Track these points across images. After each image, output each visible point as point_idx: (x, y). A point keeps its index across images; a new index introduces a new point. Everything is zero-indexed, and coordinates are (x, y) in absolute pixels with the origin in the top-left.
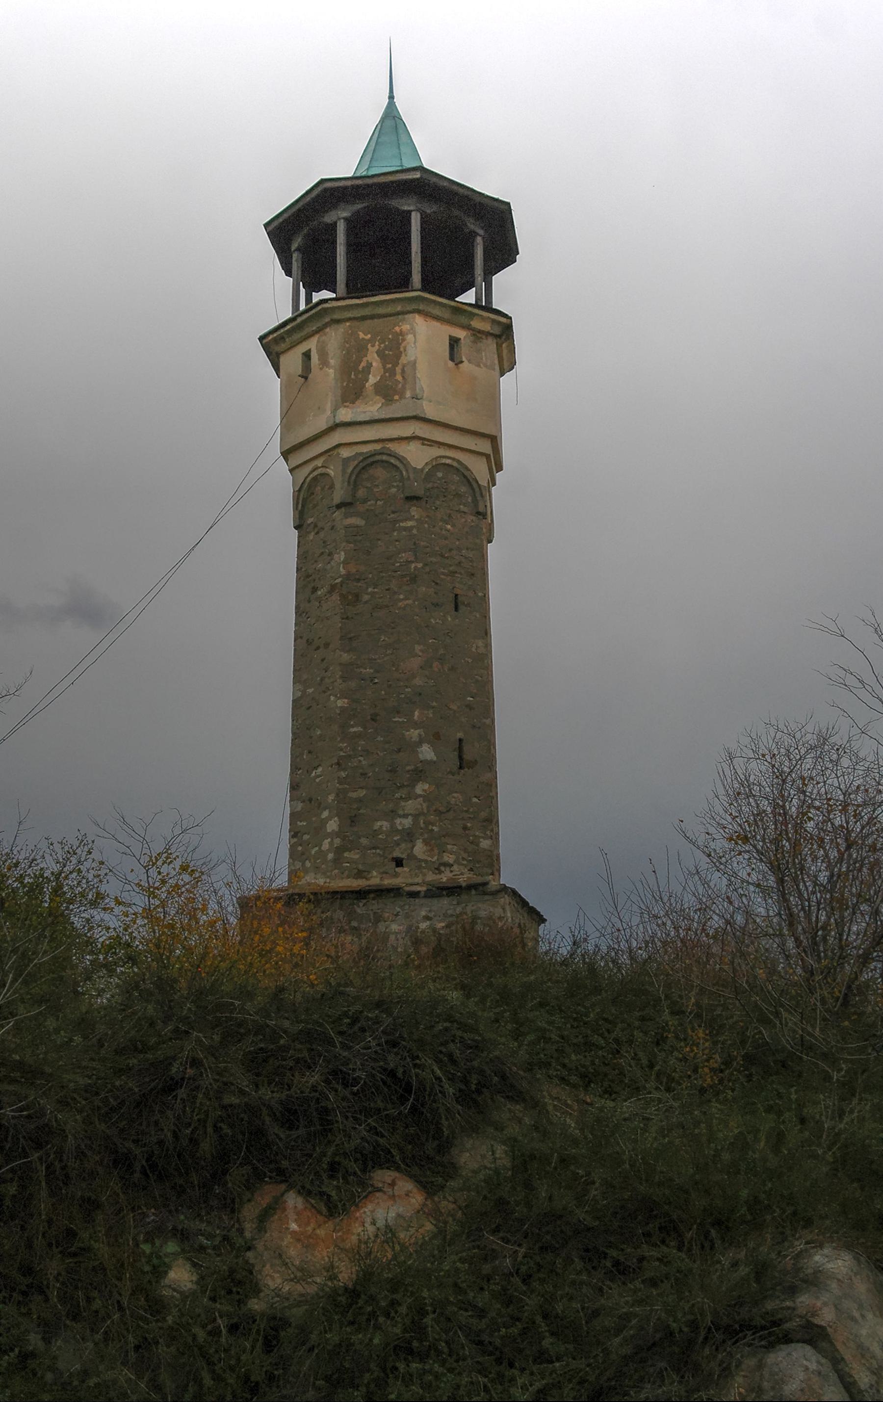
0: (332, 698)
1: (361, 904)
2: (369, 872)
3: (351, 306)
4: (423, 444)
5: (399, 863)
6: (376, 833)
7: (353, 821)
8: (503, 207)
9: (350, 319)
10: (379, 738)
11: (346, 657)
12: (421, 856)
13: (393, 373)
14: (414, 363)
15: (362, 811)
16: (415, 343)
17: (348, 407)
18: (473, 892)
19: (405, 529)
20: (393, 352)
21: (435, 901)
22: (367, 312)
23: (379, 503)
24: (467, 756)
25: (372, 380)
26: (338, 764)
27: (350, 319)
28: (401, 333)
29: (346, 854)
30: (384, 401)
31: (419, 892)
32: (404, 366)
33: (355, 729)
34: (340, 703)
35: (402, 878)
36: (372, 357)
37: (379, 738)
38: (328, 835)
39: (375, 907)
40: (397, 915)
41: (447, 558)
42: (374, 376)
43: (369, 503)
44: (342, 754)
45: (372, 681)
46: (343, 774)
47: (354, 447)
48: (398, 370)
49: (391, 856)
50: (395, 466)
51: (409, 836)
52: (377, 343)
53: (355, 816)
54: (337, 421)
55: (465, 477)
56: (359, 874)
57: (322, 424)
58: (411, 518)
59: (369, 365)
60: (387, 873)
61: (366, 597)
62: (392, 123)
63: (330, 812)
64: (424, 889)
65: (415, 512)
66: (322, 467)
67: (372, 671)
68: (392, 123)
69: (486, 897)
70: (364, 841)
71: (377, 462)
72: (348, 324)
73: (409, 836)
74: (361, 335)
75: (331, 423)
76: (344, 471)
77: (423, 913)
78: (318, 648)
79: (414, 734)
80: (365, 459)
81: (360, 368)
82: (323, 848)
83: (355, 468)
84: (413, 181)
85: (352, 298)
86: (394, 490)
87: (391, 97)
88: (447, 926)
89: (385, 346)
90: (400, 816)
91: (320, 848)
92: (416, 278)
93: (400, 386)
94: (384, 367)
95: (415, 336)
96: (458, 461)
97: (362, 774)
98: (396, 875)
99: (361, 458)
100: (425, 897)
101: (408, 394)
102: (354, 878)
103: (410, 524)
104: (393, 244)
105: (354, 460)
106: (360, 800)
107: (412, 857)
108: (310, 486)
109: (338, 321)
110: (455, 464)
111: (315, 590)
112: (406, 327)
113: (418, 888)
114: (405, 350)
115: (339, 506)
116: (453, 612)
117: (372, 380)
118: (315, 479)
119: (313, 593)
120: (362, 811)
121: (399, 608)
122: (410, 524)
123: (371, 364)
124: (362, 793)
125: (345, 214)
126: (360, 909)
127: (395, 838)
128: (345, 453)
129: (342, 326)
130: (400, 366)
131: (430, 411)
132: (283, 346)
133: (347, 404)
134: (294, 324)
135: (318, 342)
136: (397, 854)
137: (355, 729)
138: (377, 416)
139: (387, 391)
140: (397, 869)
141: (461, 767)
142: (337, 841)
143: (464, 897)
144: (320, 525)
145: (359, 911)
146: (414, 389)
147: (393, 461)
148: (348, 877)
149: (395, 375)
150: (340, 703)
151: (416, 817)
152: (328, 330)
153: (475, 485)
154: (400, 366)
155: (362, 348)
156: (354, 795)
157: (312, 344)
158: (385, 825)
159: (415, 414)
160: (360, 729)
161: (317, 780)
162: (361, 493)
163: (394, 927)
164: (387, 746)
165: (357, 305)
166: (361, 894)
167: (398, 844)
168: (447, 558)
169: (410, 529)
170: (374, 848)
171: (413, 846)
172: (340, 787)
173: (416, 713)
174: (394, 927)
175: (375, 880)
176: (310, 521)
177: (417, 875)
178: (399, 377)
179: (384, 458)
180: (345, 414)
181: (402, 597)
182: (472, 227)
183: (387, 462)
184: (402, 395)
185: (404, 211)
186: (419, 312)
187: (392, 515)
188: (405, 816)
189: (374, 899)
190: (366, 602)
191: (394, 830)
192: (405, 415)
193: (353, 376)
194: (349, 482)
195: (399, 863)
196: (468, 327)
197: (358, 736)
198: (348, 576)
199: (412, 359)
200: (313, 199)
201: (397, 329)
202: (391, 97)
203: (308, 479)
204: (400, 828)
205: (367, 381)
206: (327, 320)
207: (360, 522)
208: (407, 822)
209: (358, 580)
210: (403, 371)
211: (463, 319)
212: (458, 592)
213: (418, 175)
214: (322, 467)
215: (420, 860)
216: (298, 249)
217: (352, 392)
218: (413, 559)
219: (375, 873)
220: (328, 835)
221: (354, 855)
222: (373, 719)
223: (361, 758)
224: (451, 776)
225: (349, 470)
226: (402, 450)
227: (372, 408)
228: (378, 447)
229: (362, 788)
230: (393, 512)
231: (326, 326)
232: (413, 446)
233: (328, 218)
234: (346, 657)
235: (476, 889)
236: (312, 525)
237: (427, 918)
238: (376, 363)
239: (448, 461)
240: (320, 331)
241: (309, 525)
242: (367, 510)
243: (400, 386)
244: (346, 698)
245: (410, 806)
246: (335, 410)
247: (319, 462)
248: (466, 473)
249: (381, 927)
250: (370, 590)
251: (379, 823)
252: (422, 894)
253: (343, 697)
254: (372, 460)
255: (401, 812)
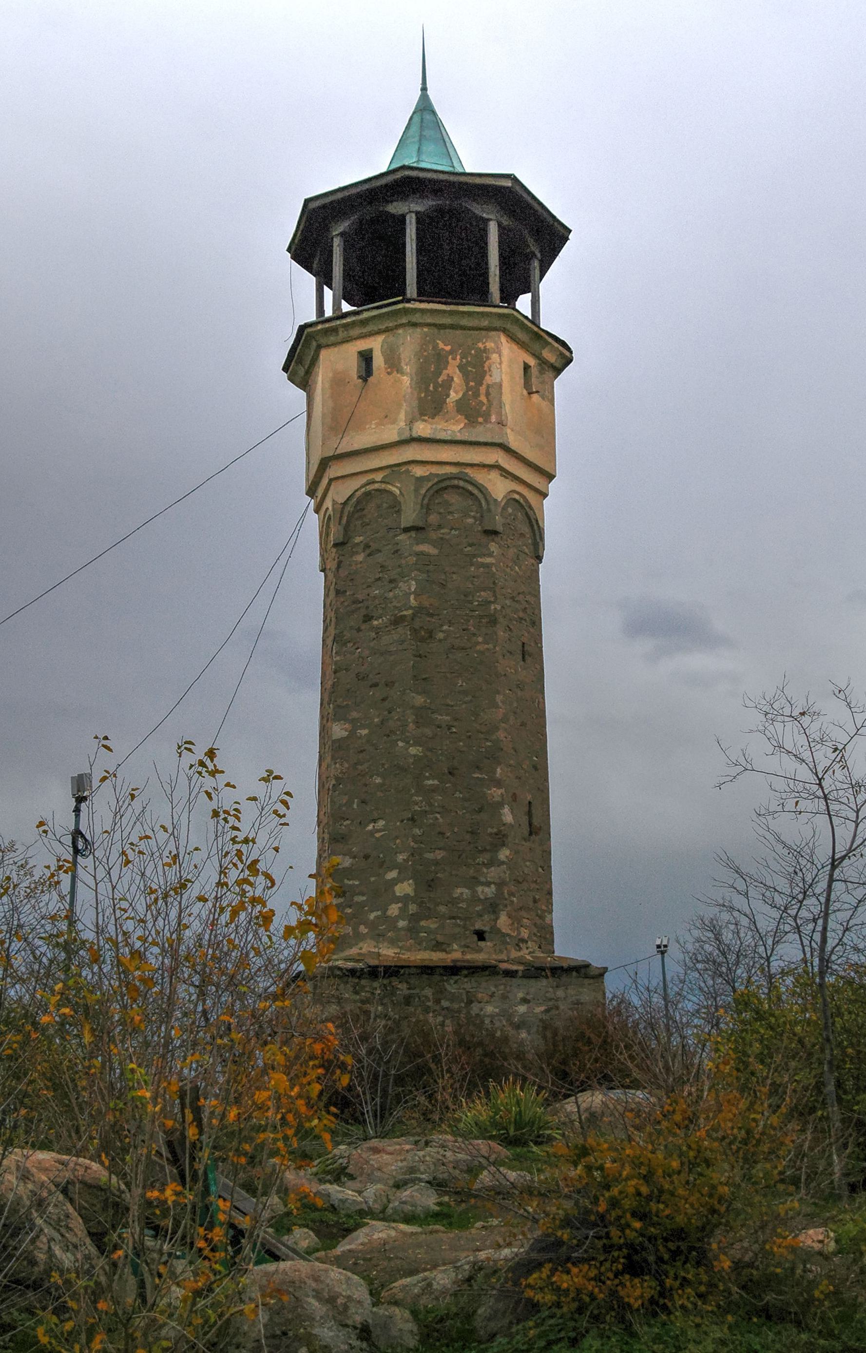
0: (400, 744)
1: (452, 982)
2: (449, 945)
3: (436, 311)
4: (501, 475)
5: (481, 935)
6: (454, 902)
7: (430, 886)
8: (562, 231)
9: (428, 325)
10: (457, 795)
11: (419, 700)
12: (505, 930)
13: (477, 394)
14: (500, 386)
15: (439, 875)
16: (500, 364)
17: (426, 421)
18: (574, 973)
19: (483, 565)
20: (476, 369)
21: (532, 982)
22: (447, 321)
23: (453, 532)
24: (535, 822)
25: (454, 396)
26: (412, 819)
27: (428, 325)
28: (485, 350)
29: (423, 923)
30: (466, 421)
31: (517, 971)
32: (488, 386)
33: (430, 782)
34: (413, 750)
35: (484, 954)
36: (453, 370)
37: (457, 795)
38: (398, 900)
39: (468, 986)
40: (492, 996)
41: (517, 601)
42: (456, 392)
43: (442, 531)
44: (417, 808)
45: (449, 729)
46: (417, 831)
47: (428, 467)
48: (483, 389)
49: (472, 928)
50: (472, 494)
51: (493, 907)
52: (458, 357)
53: (432, 880)
54: (414, 435)
55: (527, 514)
56: (438, 946)
57: (391, 434)
58: (490, 555)
59: (451, 379)
60: (468, 947)
61: (441, 635)
62: (425, 119)
63: (399, 873)
64: (521, 968)
65: (493, 547)
66: (381, 482)
67: (448, 718)
68: (425, 119)
69: (586, 981)
70: (442, 909)
71: (446, 488)
72: (426, 330)
73: (493, 907)
74: (441, 345)
75: (406, 435)
76: (416, 490)
77: (520, 995)
78: (375, 685)
79: (496, 793)
80: (439, 482)
81: (440, 380)
82: (389, 913)
83: (428, 490)
84: (504, 188)
85: (421, 301)
86: (470, 521)
87: (424, 89)
88: (547, 1011)
89: (467, 361)
90: (483, 884)
91: (384, 913)
92: (411, 289)
93: (484, 408)
94: (467, 384)
95: (500, 356)
96: (526, 501)
97: (440, 833)
98: (480, 950)
99: (436, 480)
100: (524, 977)
101: (493, 419)
102: (432, 950)
103: (488, 560)
104: (428, 248)
105: (429, 480)
106: (437, 863)
107: (496, 931)
108: (359, 502)
109: (415, 325)
110: (522, 501)
111: (368, 618)
112: (490, 345)
113: (514, 968)
114: (490, 370)
115: (406, 530)
116: (522, 663)
117: (454, 396)
118: (368, 494)
119: (365, 622)
120: (439, 875)
121: (477, 652)
122: (488, 560)
123: (452, 378)
124: (439, 855)
125: (419, 208)
126: (451, 986)
127: (477, 909)
128: (419, 471)
129: (419, 330)
130: (484, 386)
131: (514, 442)
132: (332, 339)
133: (426, 418)
134: (354, 318)
135: (383, 341)
136: (478, 926)
137: (430, 782)
138: (459, 437)
139: (471, 411)
140: (480, 943)
141: (531, 834)
142: (413, 908)
143: (564, 979)
144: (374, 546)
145: (448, 987)
146: (499, 414)
147: (470, 488)
148: (425, 949)
149: (479, 395)
150: (413, 750)
151: (500, 885)
152: (400, 331)
153: (536, 527)
154: (484, 386)
155: (441, 360)
156: (430, 856)
157: (376, 344)
158: (466, 892)
159: (501, 441)
160: (436, 782)
161: (377, 835)
162: (433, 518)
163: (490, 1009)
164: (466, 804)
165: (444, 311)
166: (453, 970)
167: (480, 915)
168: (517, 601)
169: (488, 566)
170: (454, 918)
171: (497, 919)
172: (416, 846)
173: (499, 770)
174: (490, 1009)
175: (455, 955)
176: (358, 540)
177: (501, 951)
178: (483, 398)
179: (461, 483)
180: (422, 429)
181: (480, 639)
182: (533, 249)
183: (463, 488)
184: (487, 420)
185: (482, 218)
186: (504, 331)
187: (469, 548)
188: (488, 884)
189: (466, 976)
190: (440, 641)
191: (475, 899)
192: (473, 439)
193: (431, 388)
194: (422, 505)
195: (481, 935)
196: (537, 356)
197: (434, 790)
198: (419, 611)
199: (498, 380)
200: (395, 181)
201: (480, 345)
202: (424, 89)
203: (359, 493)
204: (482, 897)
205: (448, 396)
206: (404, 320)
207: (433, 551)
208: (489, 891)
209: (432, 615)
210: (488, 394)
211: (536, 346)
212: (525, 640)
213: (509, 184)
214: (381, 482)
215: (505, 935)
216: (342, 234)
217: (431, 404)
218: (492, 599)
219: (455, 947)
220: (398, 900)
221: (432, 924)
222: (450, 773)
223: (438, 816)
224: (524, 843)
225: (423, 491)
226: (480, 477)
227: (455, 428)
228: (453, 470)
229: (440, 849)
230: (471, 545)
231: (397, 327)
232: (494, 475)
233: (396, 208)
234: (419, 700)
235: (577, 971)
236: (362, 546)
237: (525, 1001)
238: (458, 379)
239: (517, 497)
240: (388, 331)
241: (358, 544)
242: (442, 539)
243: (484, 408)
244: (420, 746)
245: (493, 873)
246: (411, 422)
247: (379, 477)
248: (530, 513)
249: (475, 1009)
250: (445, 628)
251: (459, 890)
252: (520, 974)
253: (416, 744)
254: (447, 483)
255: (483, 880)
